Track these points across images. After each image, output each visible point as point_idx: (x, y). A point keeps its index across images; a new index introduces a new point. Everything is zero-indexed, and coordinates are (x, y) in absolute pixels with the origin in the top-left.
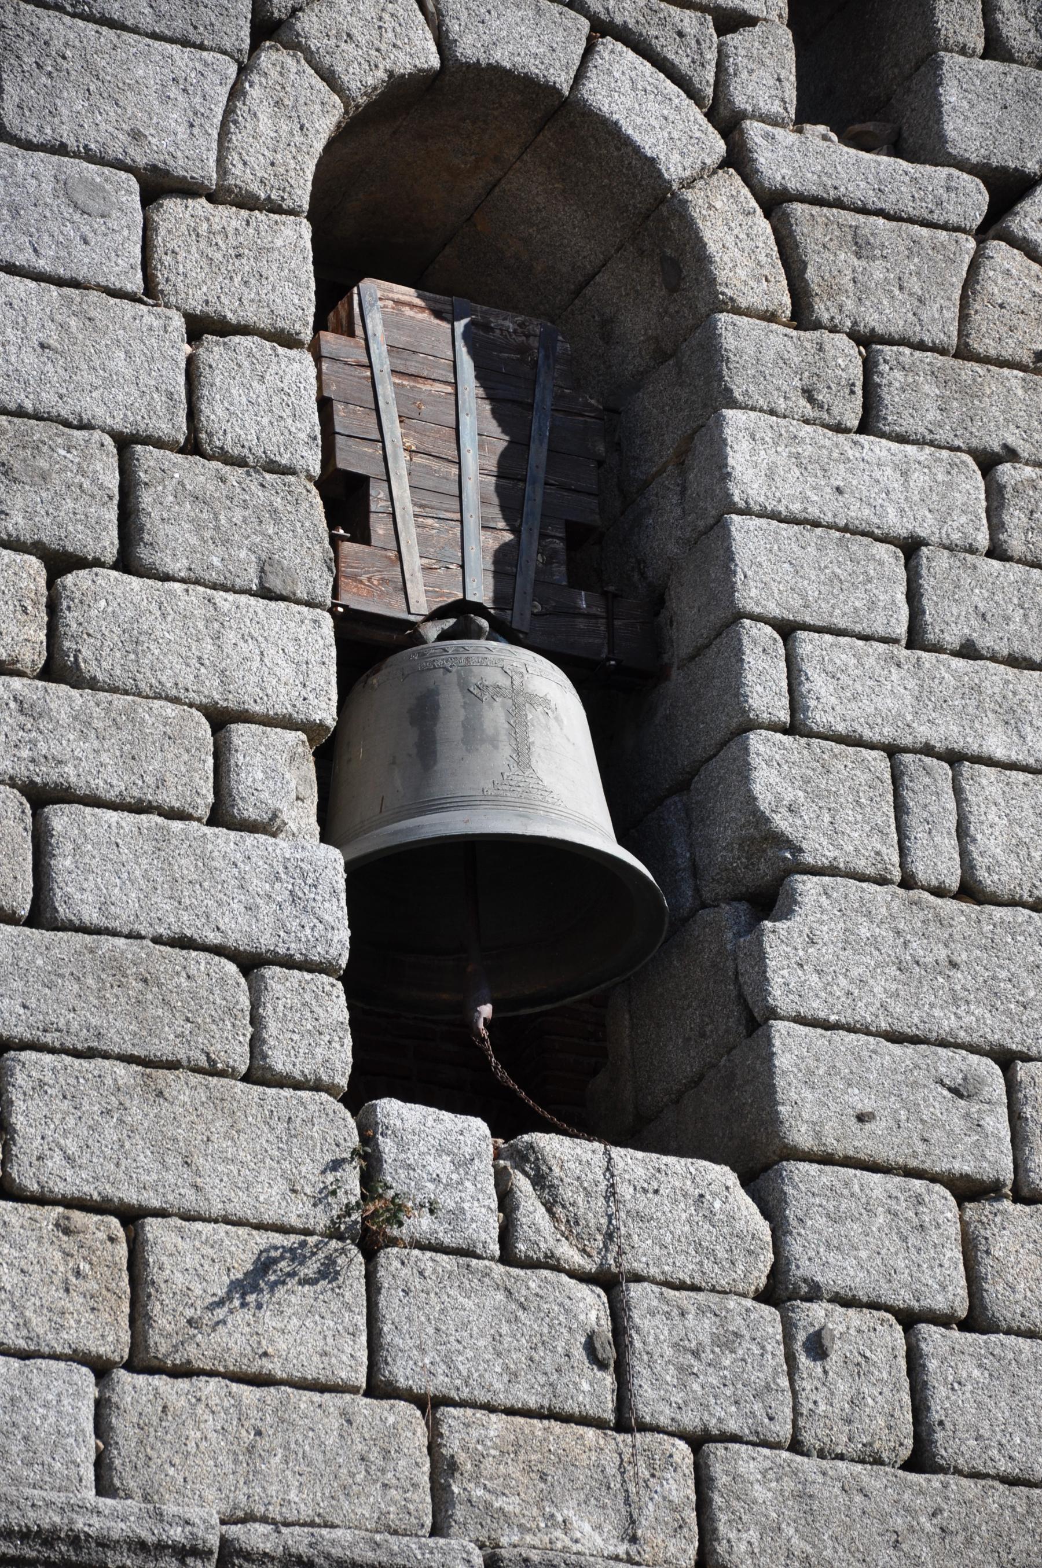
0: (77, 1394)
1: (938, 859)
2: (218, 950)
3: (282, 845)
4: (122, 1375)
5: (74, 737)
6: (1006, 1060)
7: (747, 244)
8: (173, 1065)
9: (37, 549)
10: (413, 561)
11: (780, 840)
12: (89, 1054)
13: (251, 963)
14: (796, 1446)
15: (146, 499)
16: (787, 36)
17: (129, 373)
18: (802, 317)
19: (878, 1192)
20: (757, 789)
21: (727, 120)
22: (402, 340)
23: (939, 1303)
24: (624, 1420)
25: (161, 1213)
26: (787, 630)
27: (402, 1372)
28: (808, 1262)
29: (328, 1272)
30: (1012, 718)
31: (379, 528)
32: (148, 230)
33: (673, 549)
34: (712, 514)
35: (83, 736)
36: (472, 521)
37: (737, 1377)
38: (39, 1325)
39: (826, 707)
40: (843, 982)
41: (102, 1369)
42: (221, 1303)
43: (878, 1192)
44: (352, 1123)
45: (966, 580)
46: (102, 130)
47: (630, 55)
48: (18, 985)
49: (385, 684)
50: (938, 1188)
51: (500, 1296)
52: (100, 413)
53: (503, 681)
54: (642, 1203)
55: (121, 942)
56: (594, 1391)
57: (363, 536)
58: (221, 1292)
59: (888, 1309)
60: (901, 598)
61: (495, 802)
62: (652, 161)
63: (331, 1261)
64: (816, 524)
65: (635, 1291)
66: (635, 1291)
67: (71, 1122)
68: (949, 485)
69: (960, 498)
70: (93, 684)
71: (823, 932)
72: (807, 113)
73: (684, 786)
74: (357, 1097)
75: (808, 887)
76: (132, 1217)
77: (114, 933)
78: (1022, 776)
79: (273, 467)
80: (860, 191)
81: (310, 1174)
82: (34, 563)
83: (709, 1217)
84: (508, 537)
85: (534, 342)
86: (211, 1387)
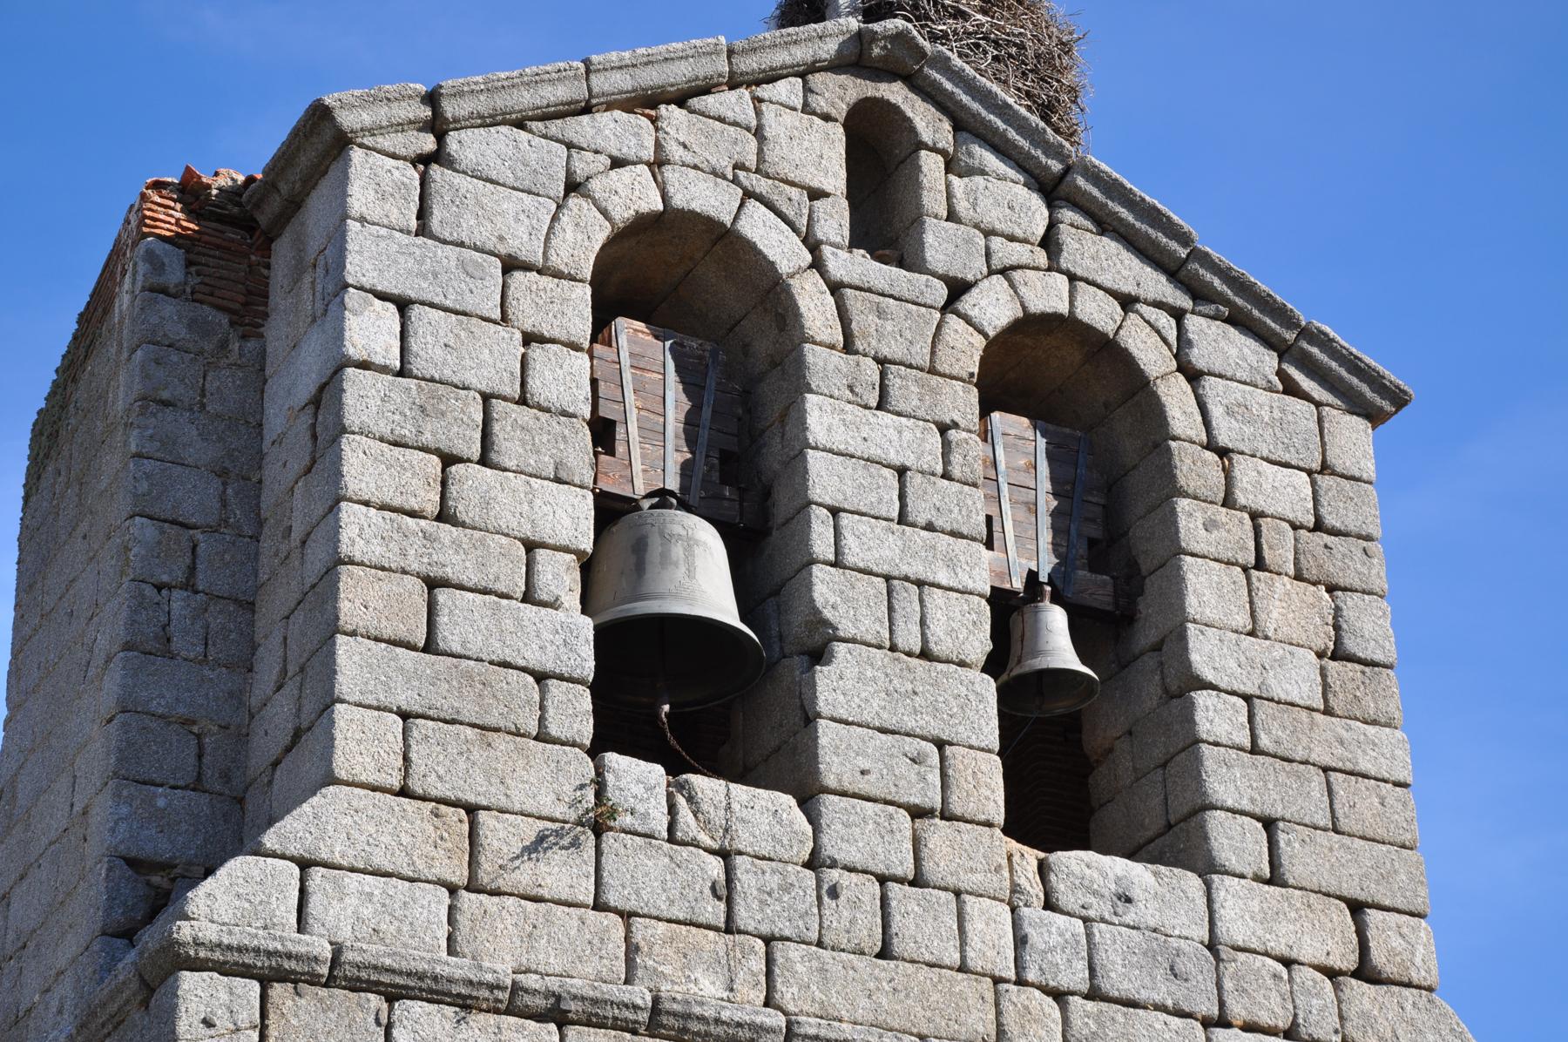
0: (439, 902)
1: (910, 637)
2: (524, 670)
3: (560, 615)
4: (463, 893)
5: (452, 553)
6: (941, 744)
7: (821, 309)
8: (497, 730)
9: (437, 452)
10: (638, 467)
11: (826, 623)
12: (453, 722)
13: (541, 677)
14: (820, 944)
15: (496, 428)
16: (845, 204)
17: (491, 361)
18: (848, 347)
19: (870, 812)
20: (816, 595)
21: (813, 245)
22: (637, 350)
23: (899, 872)
24: (730, 928)
25: (487, 808)
26: (835, 512)
27: (612, 898)
28: (830, 849)
29: (575, 844)
30: (951, 564)
31: (620, 449)
32: (505, 286)
33: (776, 466)
34: (796, 461)
35: (457, 552)
36: (670, 446)
37: (790, 907)
38: (420, 864)
39: (855, 553)
40: (857, 700)
41: (453, 890)
42: (517, 857)
43: (870, 812)
44: (591, 764)
45: (930, 490)
46: (484, 234)
47: (763, 208)
48: (416, 683)
49: (621, 532)
50: (902, 811)
51: (667, 860)
52: (474, 382)
53: (683, 533)
54: (745, 813)
55: (472, 663)
56: (714, 911)
57: (611, 451)
58: (518, 852)
59: (872, 874)
60: (896, 498)
61: (676, 596)
62: (773, 263)
63: (576, 838)
64: (852, 456)
65: (739, 860)
66: (739, 860)
67: (441, 757)
68: (923, 440)
69: (928, 447)
70: (463, 525)
71: (847, 673)
72: (854, 243)
73: (776, 592)
74: (595, 751)
75: (840, 649)
76: (472, 810)
77: (469, 658)
78: (955, 595)
79: (565, 414)
80: (881, 284)
81: (568, 790)
82: (435, 460)
83: (780, 822)
84: (689, 456)
85: (707, 354)
86: (510, 902)
